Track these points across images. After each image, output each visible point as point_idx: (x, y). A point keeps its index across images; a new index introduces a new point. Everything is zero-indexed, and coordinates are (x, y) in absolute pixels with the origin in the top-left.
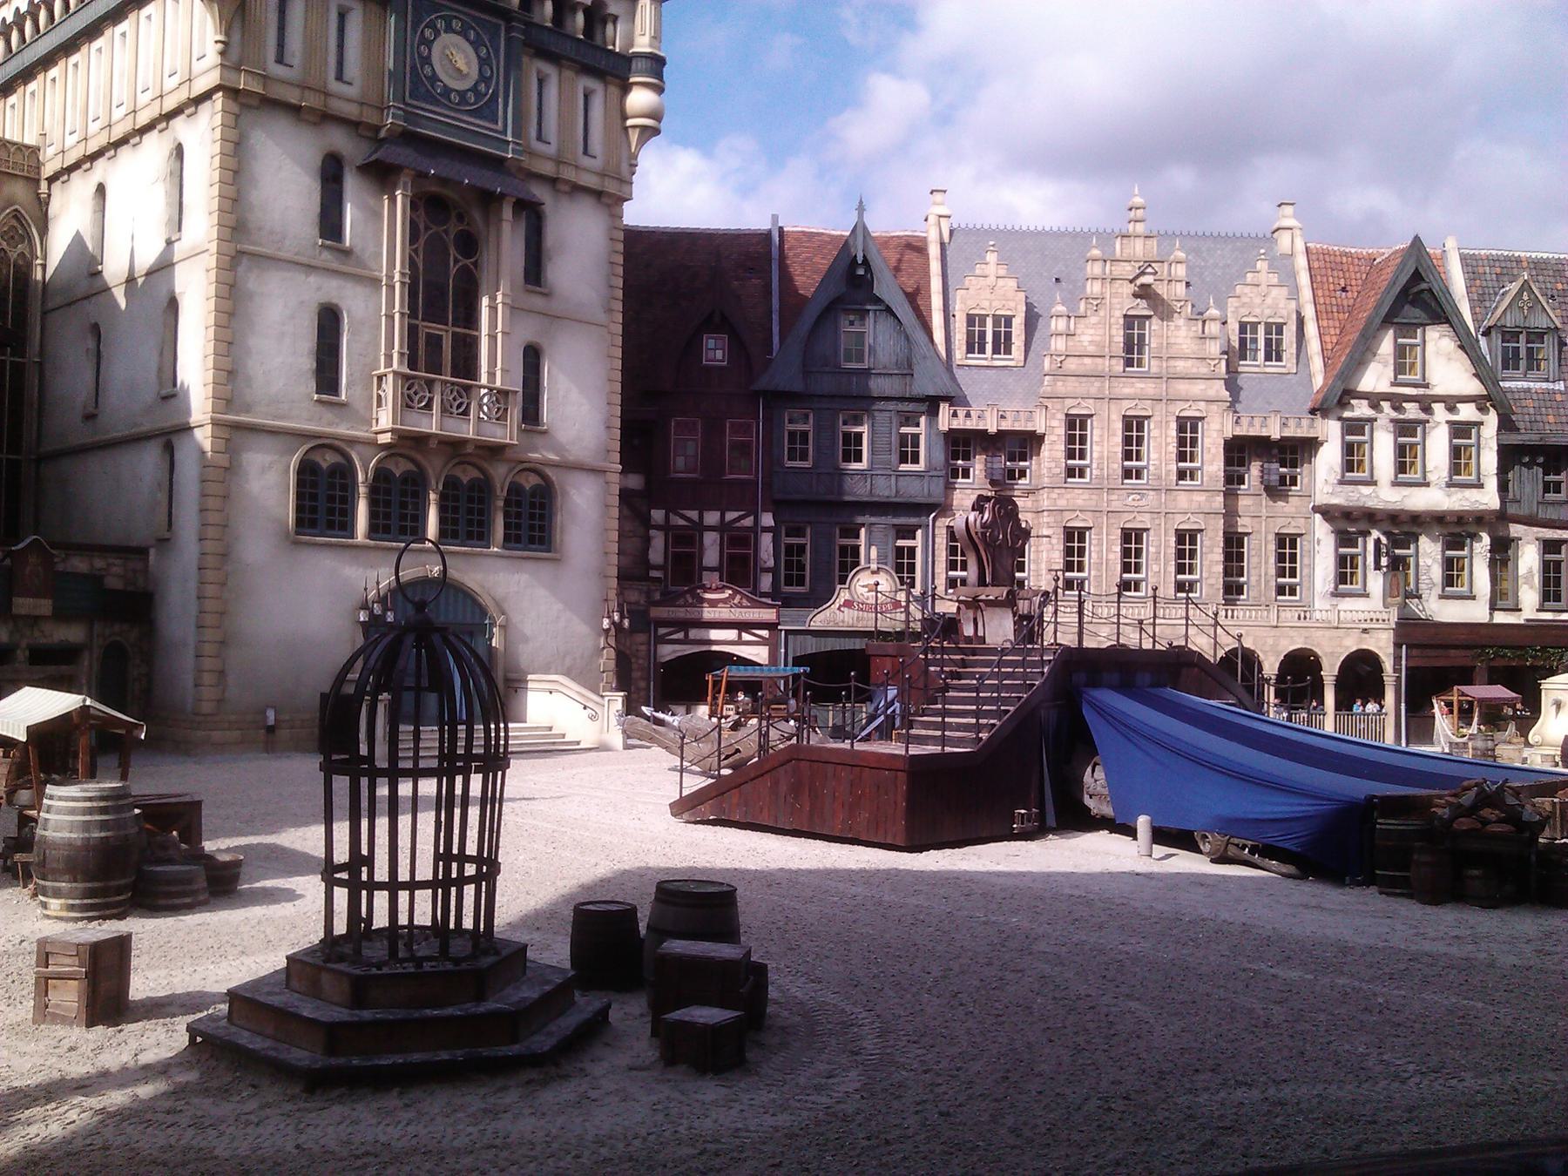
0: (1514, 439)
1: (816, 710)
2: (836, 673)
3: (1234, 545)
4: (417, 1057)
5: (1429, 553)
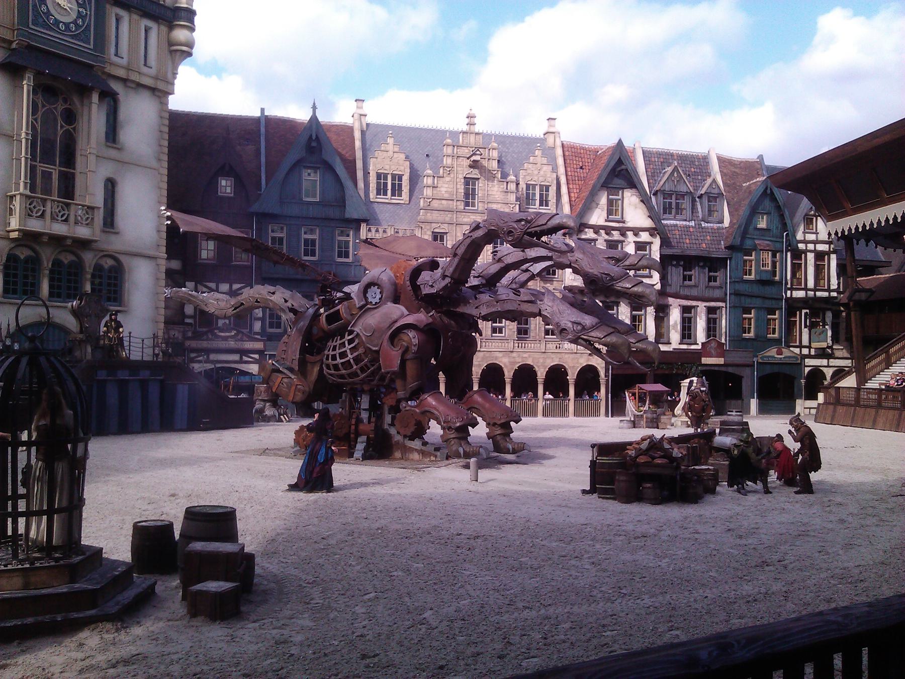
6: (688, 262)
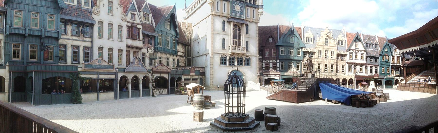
0: (367, 55)
1: (286, 85)
2: (288, 81)
3: (337, 66)
4: (236, 128)
5: (358, 67)
6: (371, 57)
